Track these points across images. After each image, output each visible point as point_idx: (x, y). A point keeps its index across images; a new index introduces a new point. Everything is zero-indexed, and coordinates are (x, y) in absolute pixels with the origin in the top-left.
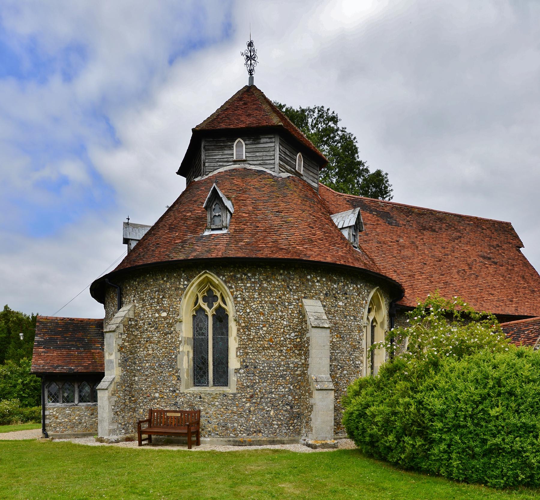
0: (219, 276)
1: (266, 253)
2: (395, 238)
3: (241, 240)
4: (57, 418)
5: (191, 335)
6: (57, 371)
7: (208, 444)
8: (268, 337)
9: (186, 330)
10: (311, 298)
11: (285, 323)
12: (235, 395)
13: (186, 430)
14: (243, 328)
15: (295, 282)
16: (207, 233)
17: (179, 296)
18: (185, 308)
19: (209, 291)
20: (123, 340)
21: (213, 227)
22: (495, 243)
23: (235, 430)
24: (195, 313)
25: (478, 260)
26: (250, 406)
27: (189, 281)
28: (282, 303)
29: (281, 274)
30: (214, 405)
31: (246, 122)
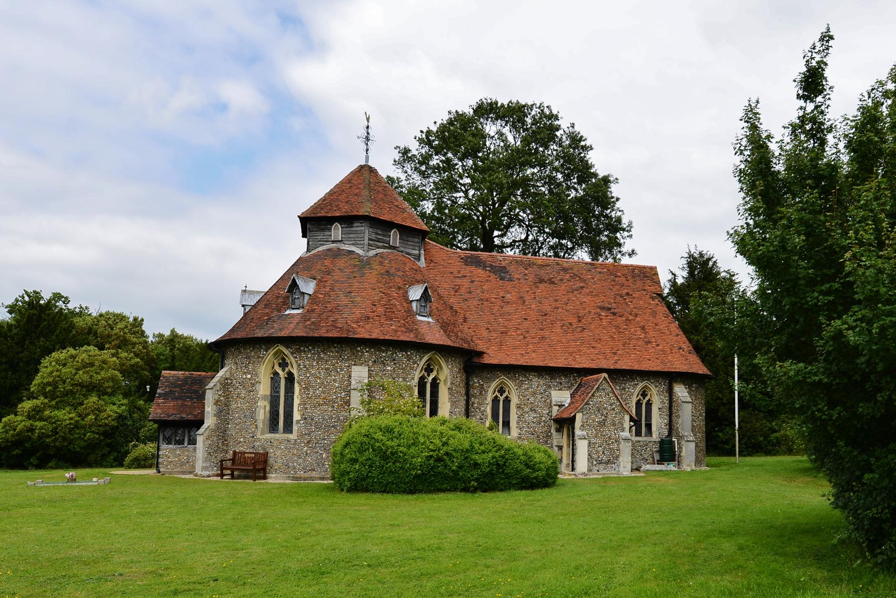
1: (322, 333)
2: (501, 294)
3: (309, 320)
5: (268, 393)
7: (274, 479)
9: (264, 388)
10: (361, 365)
13: (254, 467)
15: (347, 353)
16: (287, 312)
19: (283, 359)
22: (625, 291)
23: (294, 468)
25: (593, 311)
27: (267, 351)
31: (344, 210)
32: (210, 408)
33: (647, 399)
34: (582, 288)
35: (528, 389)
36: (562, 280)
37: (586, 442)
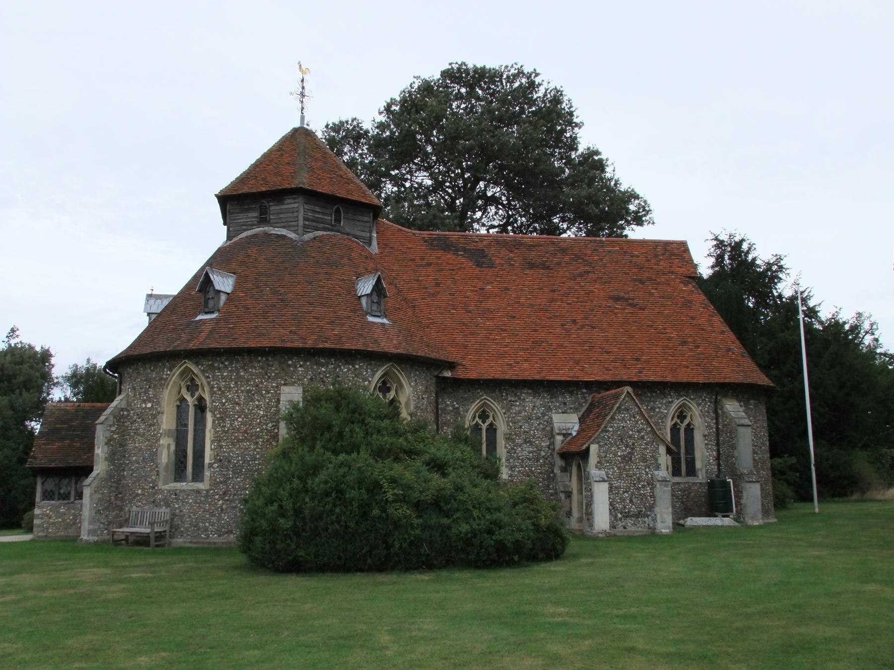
0: (198, 366)
4: (50, 518)
5: (173, 427)
6: (53, 465)
8: (243, 428)
9: (167, 421)
10: (293, 384)
11: (262, 413)
12: (207, 491)
14: (218, 419)
15: (275, 367)
16: (199, 317)
17: (162, 386)
18: (167, 400)
19: (192, 380)
20: (112, 432)
21: (207, 310)
24: (178, 403)
26: (223, 504)
27: (171, 370)
28: (259, 391)
29: (259, 361)
30: (187, 503)
32: (100, 451)
33: (686, 422)
34: (588, 272)
35: (520, 412)
36: (559, 264)
37: (605, 487)
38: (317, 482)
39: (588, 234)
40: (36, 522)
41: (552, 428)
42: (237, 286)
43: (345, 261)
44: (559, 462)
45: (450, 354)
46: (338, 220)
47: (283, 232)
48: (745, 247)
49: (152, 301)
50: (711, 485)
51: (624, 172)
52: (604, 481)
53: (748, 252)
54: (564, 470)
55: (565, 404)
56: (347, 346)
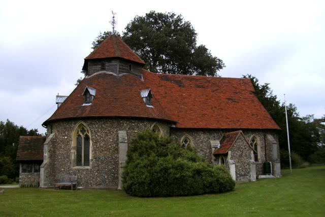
5: (76, 145)
9: (73, 144)
10: (122, 130)
15: (116, 124)
16: (84, 105)
18: (73, 135)
19: (83, 128)
27: (75, 124)
32: (46, 154)
33: (255, 143)
34: (218, 89)
37: (234, 166)
38: (157, 168)
39: (200, 74)
40: (20, 180)
41: (210, 146)
42: (97, 92)
43: (135, 84)
44: (214, 158)
45: (174, 119)
46: (130, 69)
47: (111, 73)
48: (255, 80)
49: (59, 98)
50: (264, 164)
51: (214, 52)
52: (233, 164)
53: (256, 82)
54: (215, 160)
55: (214, 137)
56: (142, 116)
